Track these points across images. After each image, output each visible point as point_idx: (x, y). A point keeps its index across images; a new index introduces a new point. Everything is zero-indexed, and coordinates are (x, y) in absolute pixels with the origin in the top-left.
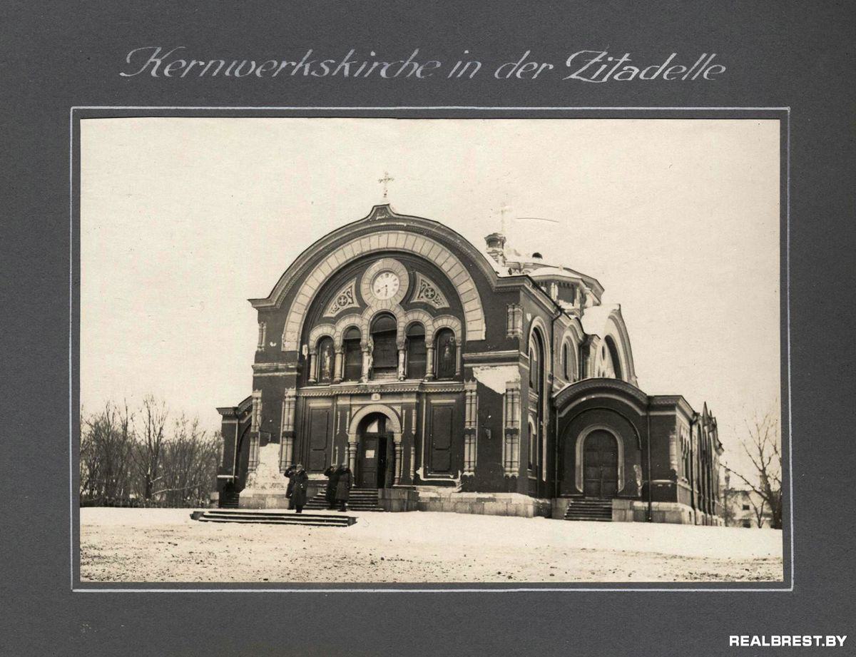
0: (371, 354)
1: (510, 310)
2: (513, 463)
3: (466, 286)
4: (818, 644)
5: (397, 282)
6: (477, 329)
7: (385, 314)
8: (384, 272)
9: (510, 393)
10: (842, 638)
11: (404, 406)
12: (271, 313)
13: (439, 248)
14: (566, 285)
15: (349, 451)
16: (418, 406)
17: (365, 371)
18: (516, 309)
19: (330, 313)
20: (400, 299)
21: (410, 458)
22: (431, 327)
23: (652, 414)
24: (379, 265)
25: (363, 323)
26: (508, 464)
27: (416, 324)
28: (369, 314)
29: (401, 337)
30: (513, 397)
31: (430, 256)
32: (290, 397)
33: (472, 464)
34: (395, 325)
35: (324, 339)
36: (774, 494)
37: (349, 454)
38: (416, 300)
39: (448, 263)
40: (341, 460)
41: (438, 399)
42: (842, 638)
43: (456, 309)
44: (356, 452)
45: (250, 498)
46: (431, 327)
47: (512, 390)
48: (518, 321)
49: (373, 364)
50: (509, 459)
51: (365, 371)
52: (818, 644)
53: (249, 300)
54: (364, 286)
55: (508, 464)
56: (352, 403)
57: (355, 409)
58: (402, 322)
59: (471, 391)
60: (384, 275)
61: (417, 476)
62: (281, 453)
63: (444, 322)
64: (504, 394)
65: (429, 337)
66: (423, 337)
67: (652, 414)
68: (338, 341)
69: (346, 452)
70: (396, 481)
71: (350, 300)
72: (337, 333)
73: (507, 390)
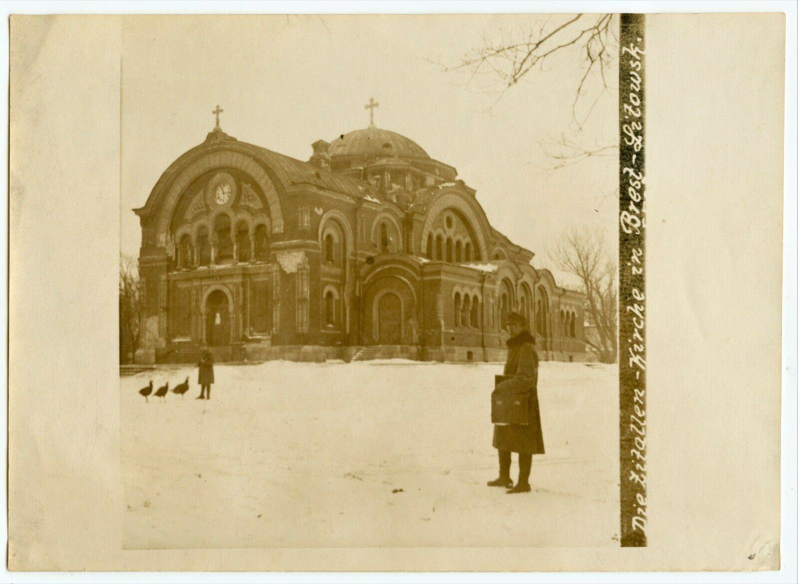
1: (300, 209)
2: (303, 324)
3: (271, 194)
5: (230, 190)
6: (278, 227)
7: (223, 215)
9: (300, 272)
11: (235, 284)
12: (148, 216)
13: (262, 172)
15: (201, 319)
16: (243, 284)
17: (213, 259)
18: (303, 208)
19: (189, 216)
20: (231, 204)
22: (252, 225)
23: (426, 278)
24: (218, 177)
25: (208, 222)
26: (300, 324)
27: (242, 222)
28: (213, 215)
30: (302, 274)
31: (252, 174)
33: (278, 325)
34: (230, 223)
35: (185, 237)
38: (242, 203)
39: (264, 181)
40: (447, 272)
41: (224, 270)
43: (266, 210)
44: (207, 320)
45: (140, 357)
46: (252, 225)
47: (301, 269)
48: (305, 215)
49: (219, 253)
50: (300, 321)
51: (213, 259)
54: (209, 194)
57: (204, 288)
58: (234, 219)
61: (244, 336)
62: (159, 323)
63: (262, 219)
64: (296, 273)
65: (251, 231)
67: (426, 278)
68: (194, 238)
70: (231, 339)
73: (298, 270)
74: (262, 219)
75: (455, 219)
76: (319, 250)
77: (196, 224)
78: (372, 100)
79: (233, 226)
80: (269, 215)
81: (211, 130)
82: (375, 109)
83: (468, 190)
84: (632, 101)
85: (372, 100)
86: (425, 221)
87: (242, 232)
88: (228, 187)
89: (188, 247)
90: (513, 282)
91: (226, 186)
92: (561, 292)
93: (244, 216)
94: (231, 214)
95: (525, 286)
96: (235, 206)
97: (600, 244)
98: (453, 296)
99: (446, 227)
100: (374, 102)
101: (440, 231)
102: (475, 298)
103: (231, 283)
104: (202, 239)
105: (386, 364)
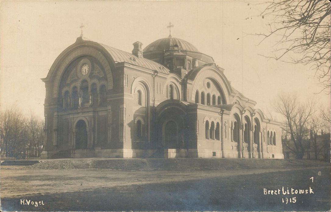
0: (81, 97)
4: (24, 204)
7: (85, 81)
8: (84, 64)
10: (28, 201)
14: (178, 59)
19: (68, 82)
21: (234, 128)
24: (82, 61)
25: (78, 84)
29: (90, 90)
32: (55, 116)
35: (67, 92)
36: (120, 150)
37: (74, 137)
42: (28, 201)
46: (99, 84)
52: (24, 204)
53: (41, 79)
55: (121, 137)
56: (74, 116)
59: (110, 109)
60: (85, 65)
66: (96, 89)
68: (71, 93)
69: (73, 136)
71: (74, 76)
72: (69, 89)
74: (103, 82)
75: (212, 84)
76: (133, 98)
77: (72, 86)
78: (170, 23)
79: (89, 86)
80: (107, 80)
81: (79, 36)
82: (172, 28)
83: (220, 69)
84: (295, 192)
85: (170, 23)
86: (194, 84)
87: (94, 90)
88: (88, 66)
89: (68, 98)
90: (240, 116)
91: (86, 65)
92: (267, 121)
93: (95, 81)
94: (89, 80)
95: (247, 118)
96: (91, 75)
97: (295, 99)
98: (205, 123)
99: (207, 88)
100: (171, 25)
101: (203, 90)
102: (218, 124)
103: (87, 116)
104: (75, 92)
105: (262, 147)
